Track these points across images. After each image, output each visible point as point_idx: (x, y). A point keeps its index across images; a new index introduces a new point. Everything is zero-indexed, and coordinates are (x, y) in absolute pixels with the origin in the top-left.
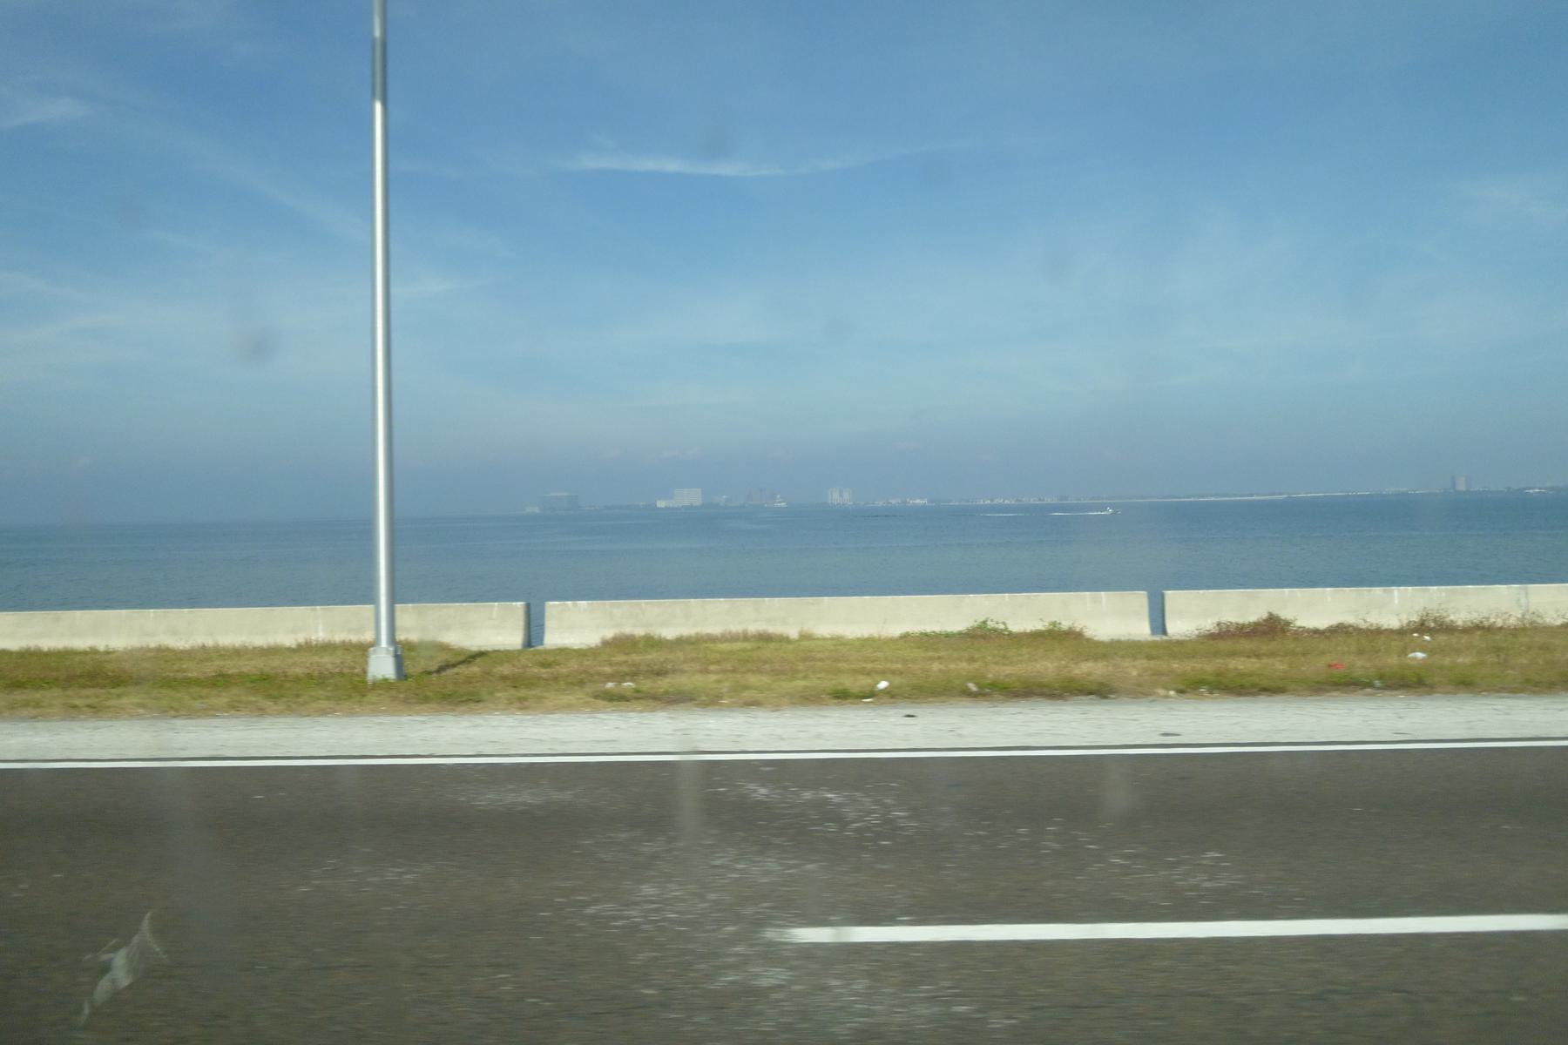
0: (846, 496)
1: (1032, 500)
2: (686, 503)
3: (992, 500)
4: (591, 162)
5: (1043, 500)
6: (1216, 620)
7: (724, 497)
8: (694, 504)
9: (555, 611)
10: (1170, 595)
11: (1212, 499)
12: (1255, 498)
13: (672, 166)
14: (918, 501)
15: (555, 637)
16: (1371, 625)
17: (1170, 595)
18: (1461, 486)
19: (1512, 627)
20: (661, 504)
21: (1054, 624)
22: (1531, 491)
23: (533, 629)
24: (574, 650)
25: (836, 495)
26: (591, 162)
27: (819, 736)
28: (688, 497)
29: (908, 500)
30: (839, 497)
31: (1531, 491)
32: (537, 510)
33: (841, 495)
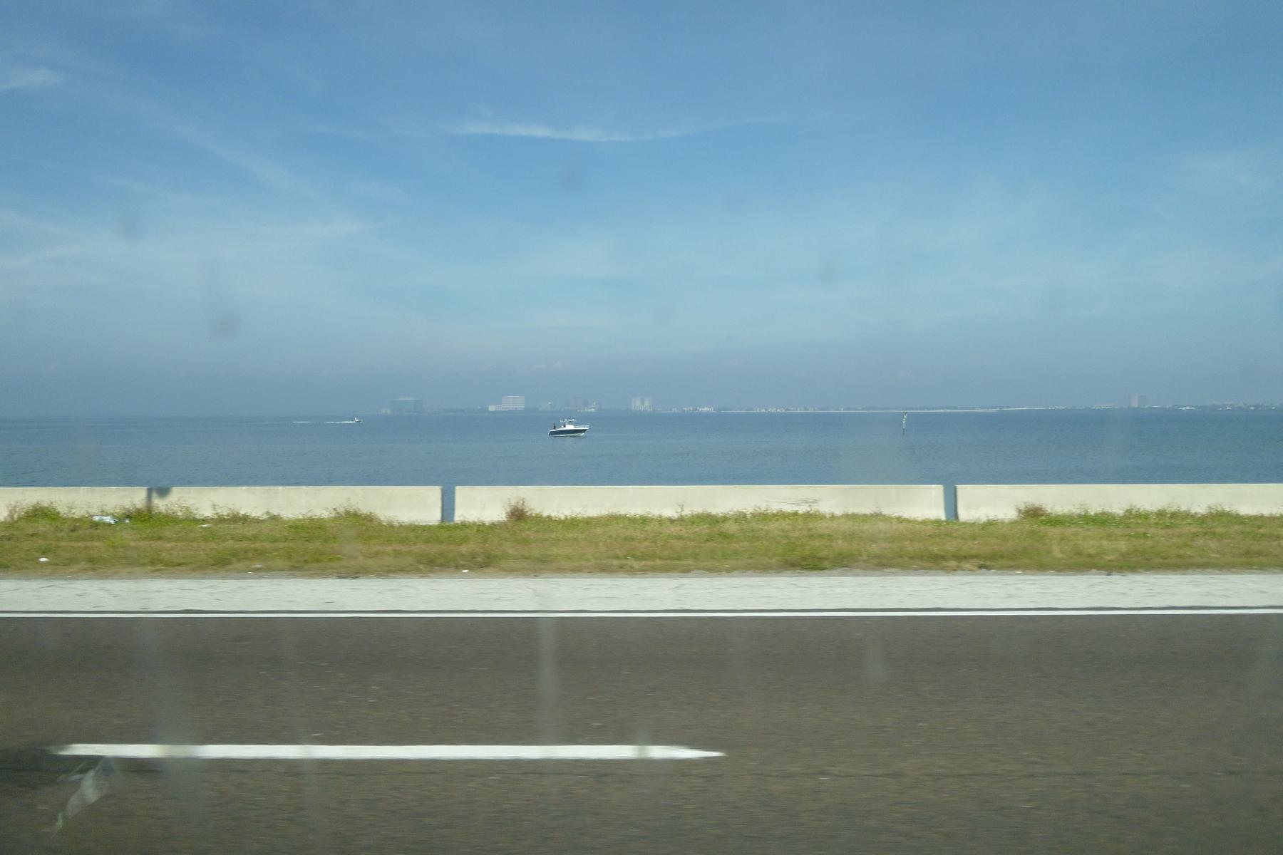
0: (647, 403)
1: (798, 409)
2: (512, 408)
3: (766, 409)
4: (474, 128)
5: (752, 409)
6: (648, 510)
7: (550, 403)
8: (518, 409)
9: (463, 494)
10: (960, 488)
11: (942, 411)
12: (976, 411)
13: (540, 132)
14: (706, 409)
15: (461, 515)
16: (653, 515)
17: (960, 488)
18: (1135, 404)
19: (487, 524)
20: (492, 408)
21: (371, 513)
22: (1184, 409)
23: (448, 505)
24: (560, 522)
25: (638, 403)
26: (474, 128)
27: (1009, 596)
28: (513, 403)
29: (698, 408)
30: (640, 404)
31: (1184, 409)
32: (389, 412)
33: (643, 403)
